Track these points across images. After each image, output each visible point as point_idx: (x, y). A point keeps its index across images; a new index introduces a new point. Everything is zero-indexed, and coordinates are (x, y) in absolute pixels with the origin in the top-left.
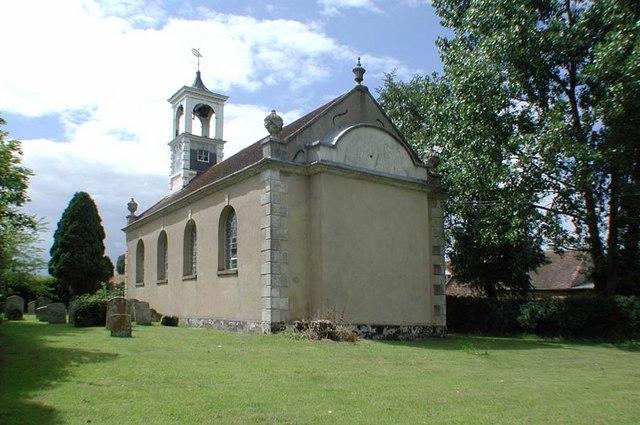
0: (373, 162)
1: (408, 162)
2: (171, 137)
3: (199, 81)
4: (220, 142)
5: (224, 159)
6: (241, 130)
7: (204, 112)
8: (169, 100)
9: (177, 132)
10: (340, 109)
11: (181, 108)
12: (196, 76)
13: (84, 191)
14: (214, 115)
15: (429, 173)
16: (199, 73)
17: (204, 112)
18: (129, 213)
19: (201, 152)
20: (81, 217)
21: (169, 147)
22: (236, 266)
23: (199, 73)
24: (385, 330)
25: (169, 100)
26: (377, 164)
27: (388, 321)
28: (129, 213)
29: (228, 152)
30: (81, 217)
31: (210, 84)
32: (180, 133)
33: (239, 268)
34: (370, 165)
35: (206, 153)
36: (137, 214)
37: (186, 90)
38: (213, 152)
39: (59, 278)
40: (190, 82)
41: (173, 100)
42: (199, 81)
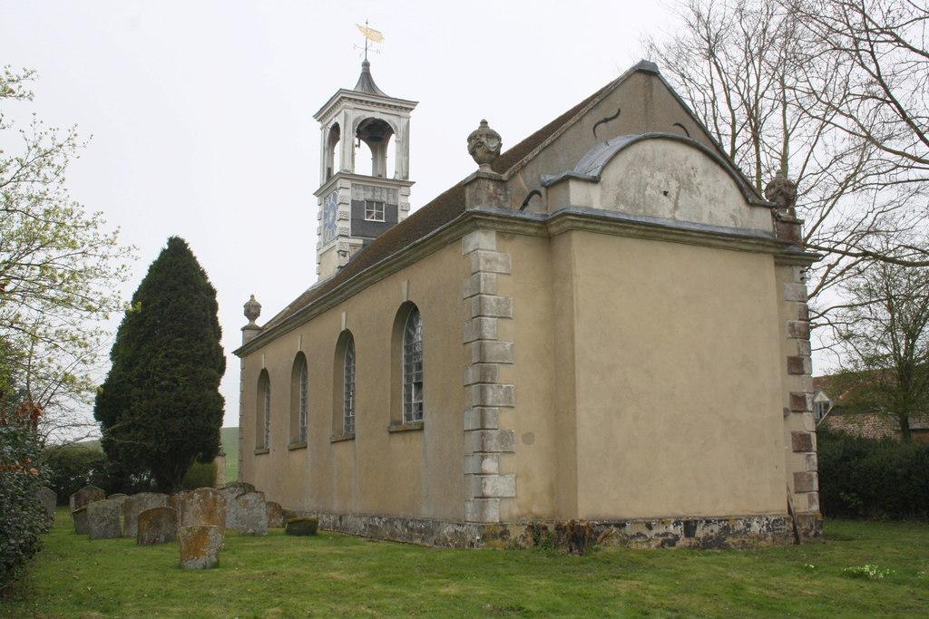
0: (671, 205)
1: (734, 198)
2: (317, 181)
3: (366, 77)
4: (404, 182)
5: (410, 213)
6: (434, 167)
7: (375, 133)
8: (315, 116)
9: (330, 170)
10: (607, 110)
11: (336, 128)
12: (360, 70)
13: (181, 237)
14: (393, 137)
15: (776, 217)
16: (366, 65)
17: (375, 133)
18: (246, 322)
19: (370, 203)
20: (176, 288)
21: (316, 199)
22: (420, 415)
23: (366, 65)
24: (699, 528)
25: (315, 116)
26: (676, 207)
27: (708, 510)
28: (246, 322)
29: (417, 199)
30: (176, 288)
31: (387, 84)
32: (336, 170)
33: (426, 419)
34: (664, 213)
35: (380, 204)
36: (260, 322)
37: (342, 97)
38: (391, 202)
39: (111, 458)
40: (351, 82)
41: (322, 115)
42: (366, 77)
